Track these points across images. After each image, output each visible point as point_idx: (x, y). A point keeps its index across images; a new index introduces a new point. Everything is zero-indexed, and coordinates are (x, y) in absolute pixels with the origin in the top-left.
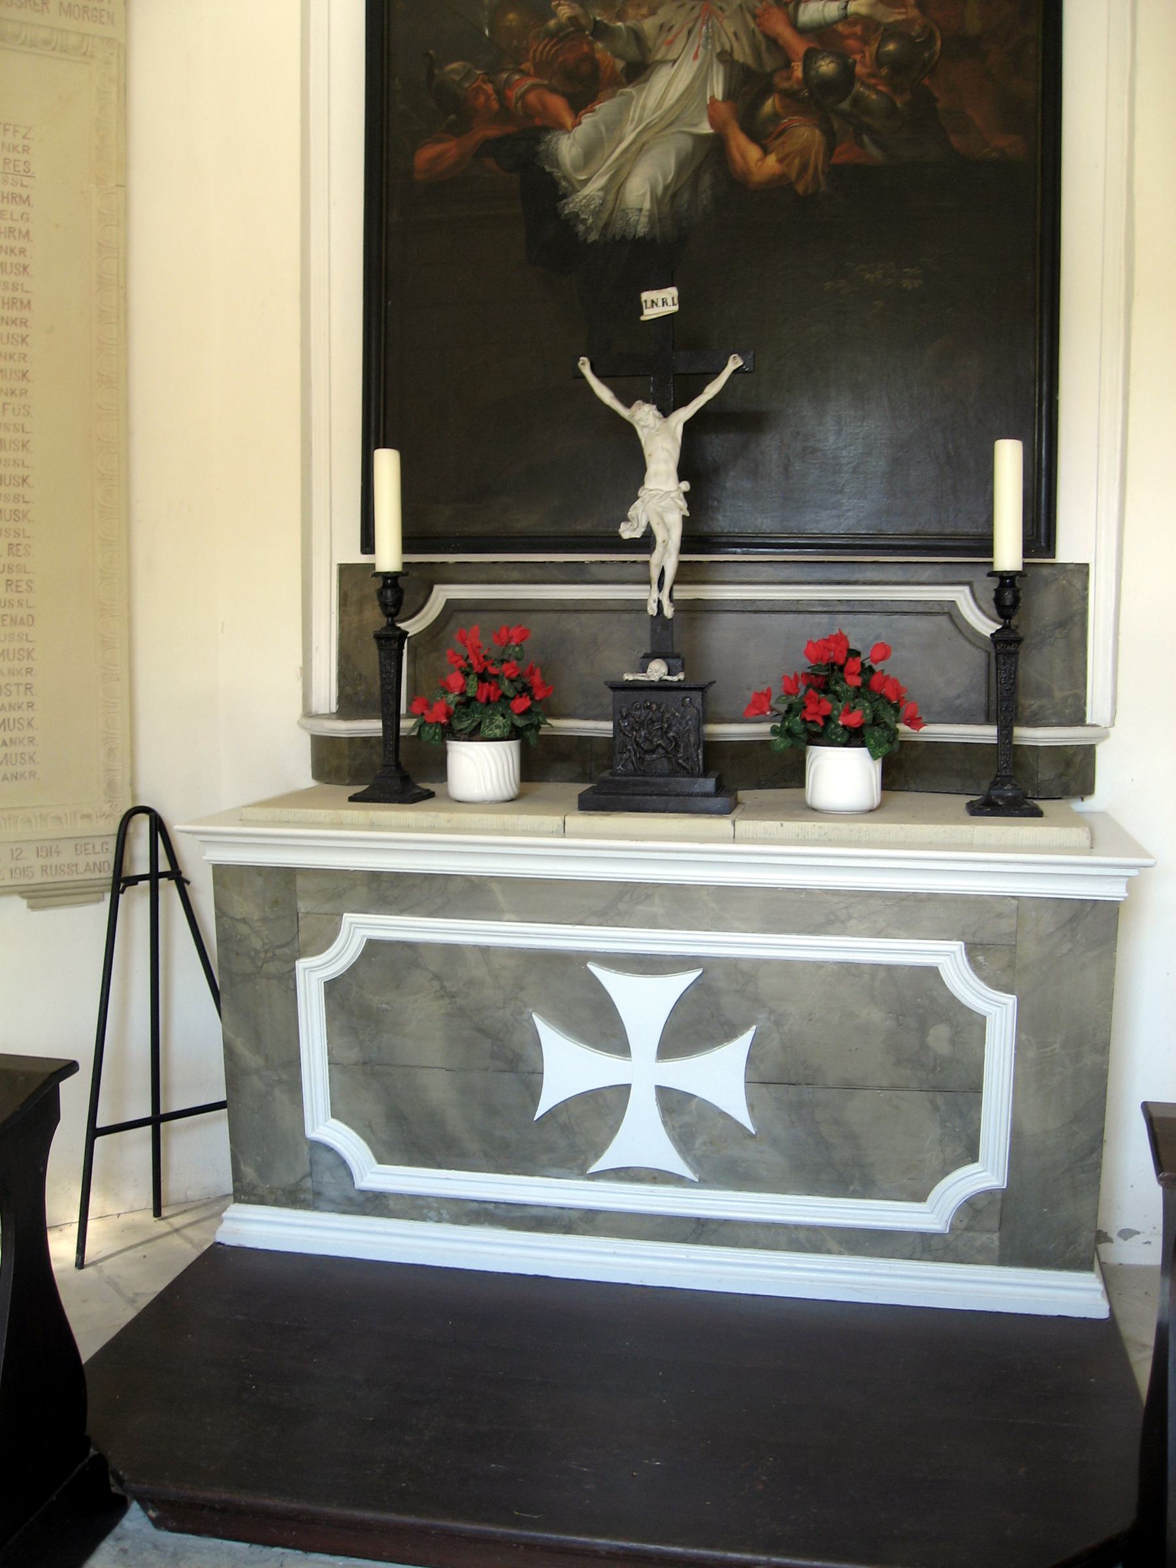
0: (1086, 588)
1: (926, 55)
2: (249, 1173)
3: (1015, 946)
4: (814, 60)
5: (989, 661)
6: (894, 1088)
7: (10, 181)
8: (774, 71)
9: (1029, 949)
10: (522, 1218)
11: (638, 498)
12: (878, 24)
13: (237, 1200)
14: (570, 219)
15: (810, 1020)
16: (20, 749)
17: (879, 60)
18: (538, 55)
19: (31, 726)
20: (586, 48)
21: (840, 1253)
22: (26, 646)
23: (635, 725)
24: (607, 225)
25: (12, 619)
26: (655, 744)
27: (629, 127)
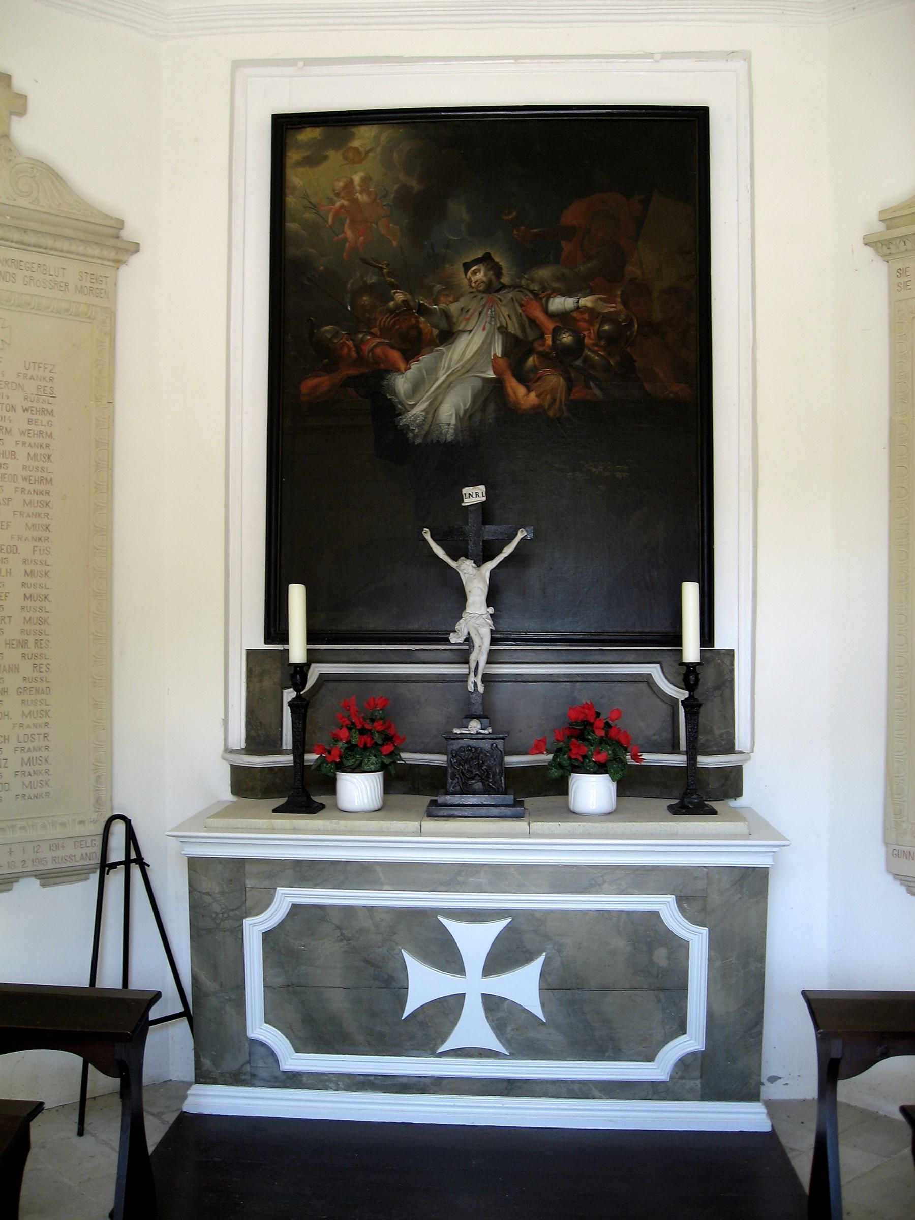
0: (732, 664)
1: (628, 333)
2: (207, 1063)
3: (706, 897)
4: (559, 334)
5: (673, 712)
6: (633, 989)
7: (41, 400)
8: (534, 340)
9: (715, 898)
10: (394, 1085)
11: (462, 617)
12: (599, 313)
13: (197, 1082)
14: (403, 429)
15: (580, 948)
16: (40, 778)
17: (599, 335)
18: (382, 324)
19: (47, 761)
20: (413, 321)
21: (601, 1098)
22: (44, 708)
23: (461, 762)
24: (428, 433)
25: (36, 690)
26: (474, 773)
27: (442, 372)
